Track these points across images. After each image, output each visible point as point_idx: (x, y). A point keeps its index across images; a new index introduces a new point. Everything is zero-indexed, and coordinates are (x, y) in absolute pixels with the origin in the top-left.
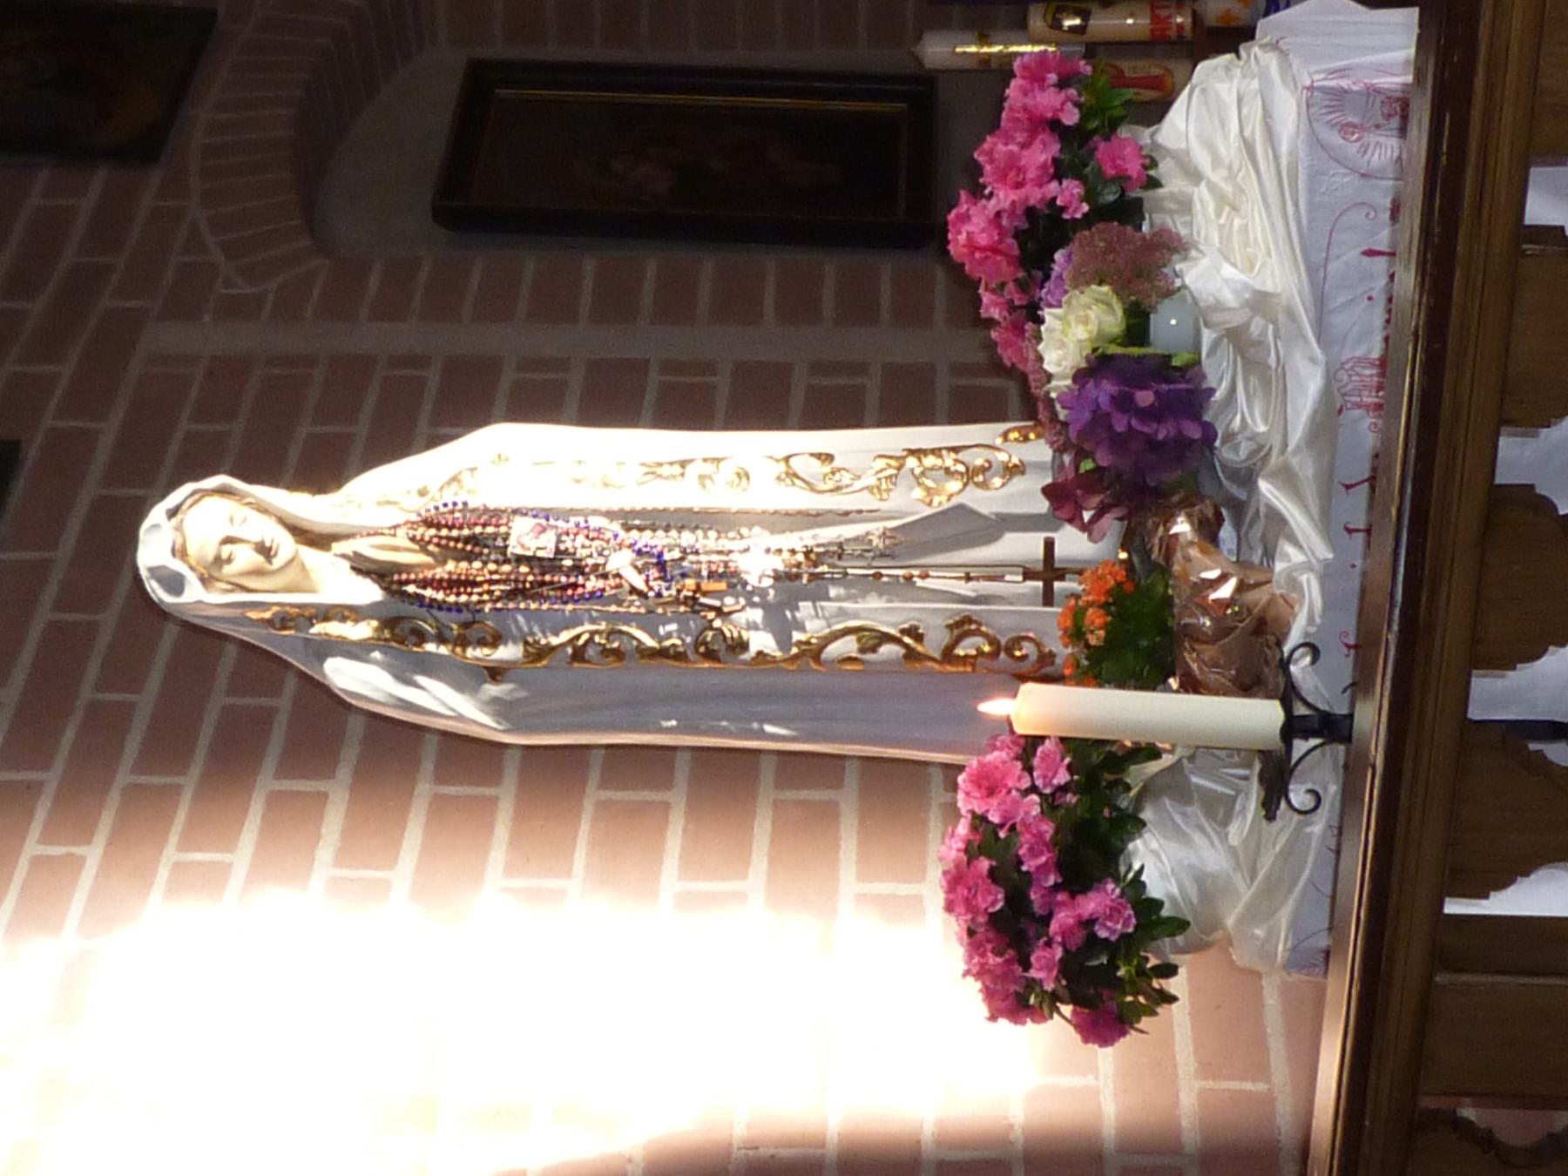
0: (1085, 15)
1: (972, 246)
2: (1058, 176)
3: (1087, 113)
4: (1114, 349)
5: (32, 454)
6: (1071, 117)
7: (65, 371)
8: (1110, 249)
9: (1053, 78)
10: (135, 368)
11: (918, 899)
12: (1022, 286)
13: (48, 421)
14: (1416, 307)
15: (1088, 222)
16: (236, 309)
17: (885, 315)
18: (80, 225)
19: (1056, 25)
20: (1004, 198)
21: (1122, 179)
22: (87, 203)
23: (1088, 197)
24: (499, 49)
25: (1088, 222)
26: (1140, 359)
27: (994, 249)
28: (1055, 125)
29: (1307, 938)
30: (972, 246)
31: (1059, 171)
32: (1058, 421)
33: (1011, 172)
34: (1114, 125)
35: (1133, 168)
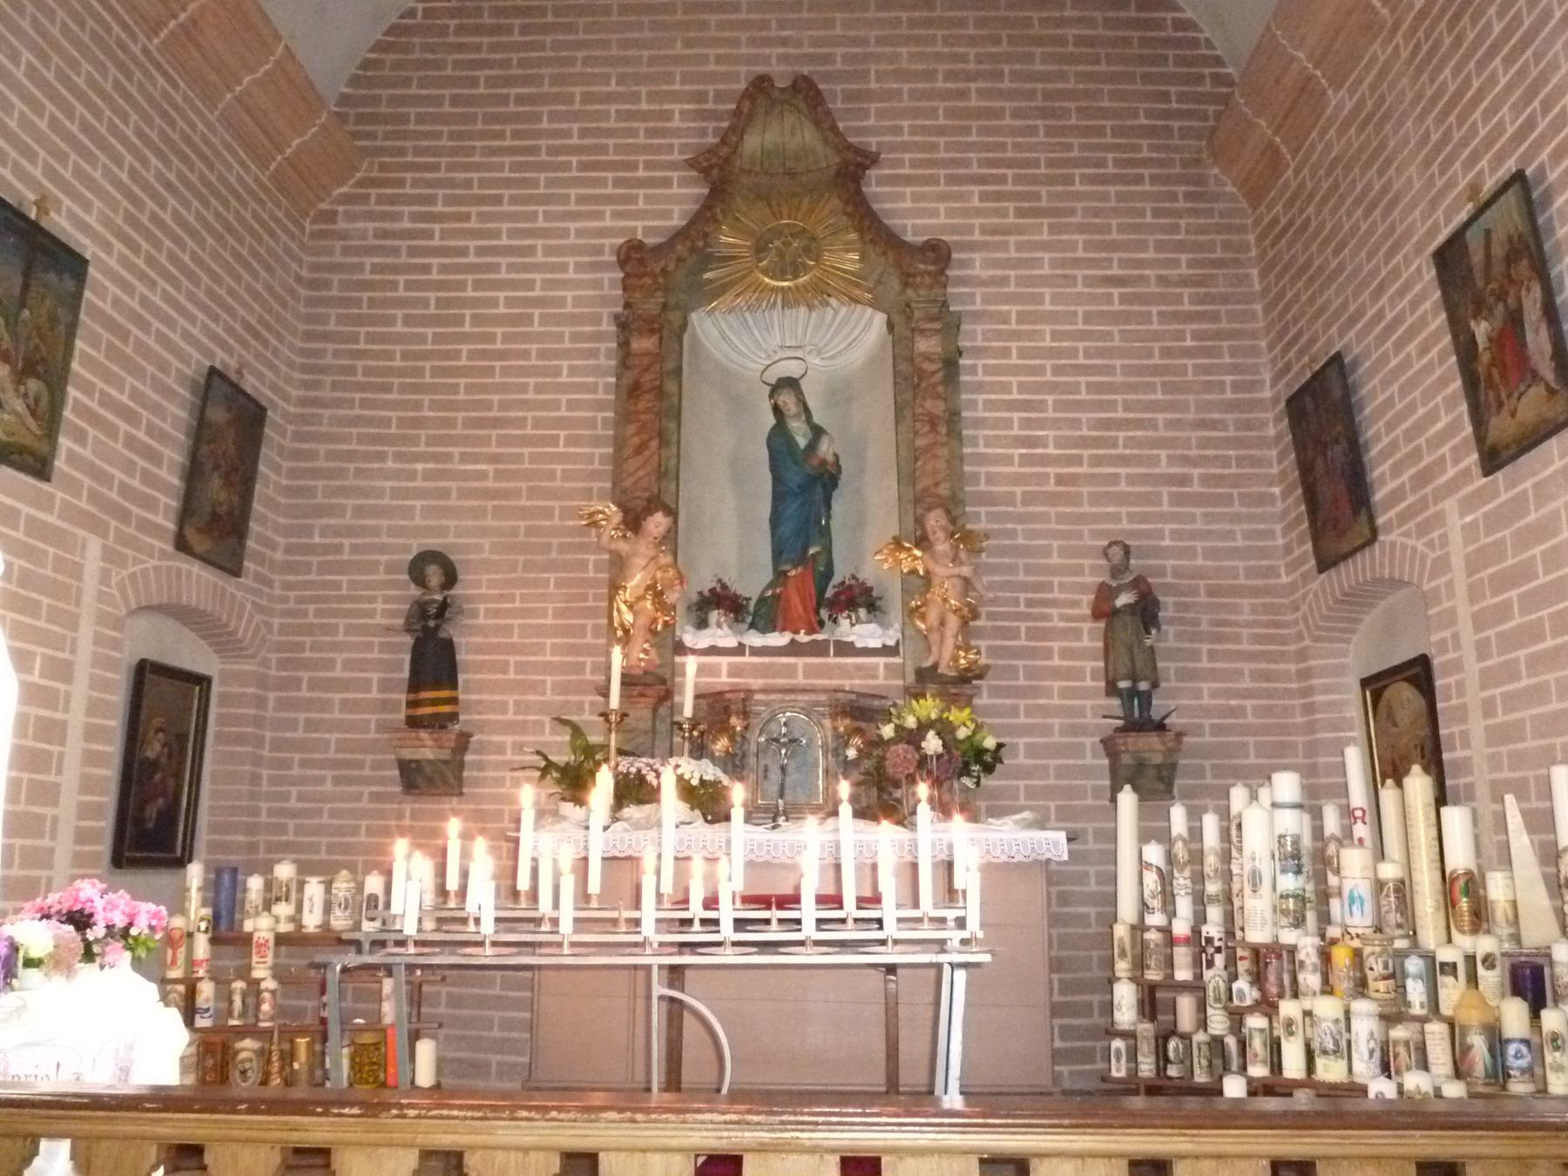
0: (206, 931)
1: (78, 890)
2: (108, 927)
3: (136, 939)
4: (21, 954)
5: (44, 486)
6: (134, 931)
7: (83, 504)
8: (70, 950)
9: (154, 923)
10: (81, 533)
11: (25, 736)
12: (59, 912)
13: (60, 495)
14: (689, 1117)
15: (85, 940)
16: (105, 577)
17: (78, 848)
18: (150, 516)
19: (202, 919)
20: (99, 904)
21: (103, 955)
22: (159, 519)
23: (97, 941)
24: (216, 689)
25: (85, 940)
26: (16, 965)
27: (76, 900)
28: (131, 924)
29: (1089, 1093)
30: (78, 890)
31: (109, 927)
32: (919, 748)
33: (112, 906)
34: (132, 949)
35: (108, 959)
